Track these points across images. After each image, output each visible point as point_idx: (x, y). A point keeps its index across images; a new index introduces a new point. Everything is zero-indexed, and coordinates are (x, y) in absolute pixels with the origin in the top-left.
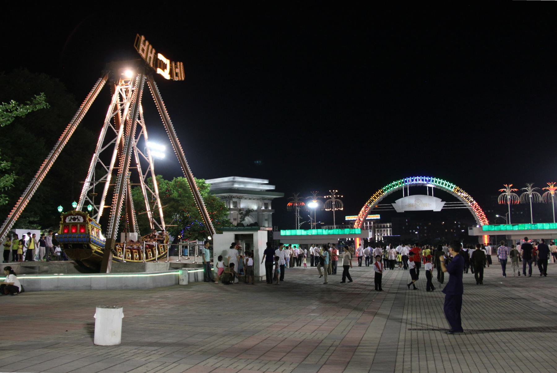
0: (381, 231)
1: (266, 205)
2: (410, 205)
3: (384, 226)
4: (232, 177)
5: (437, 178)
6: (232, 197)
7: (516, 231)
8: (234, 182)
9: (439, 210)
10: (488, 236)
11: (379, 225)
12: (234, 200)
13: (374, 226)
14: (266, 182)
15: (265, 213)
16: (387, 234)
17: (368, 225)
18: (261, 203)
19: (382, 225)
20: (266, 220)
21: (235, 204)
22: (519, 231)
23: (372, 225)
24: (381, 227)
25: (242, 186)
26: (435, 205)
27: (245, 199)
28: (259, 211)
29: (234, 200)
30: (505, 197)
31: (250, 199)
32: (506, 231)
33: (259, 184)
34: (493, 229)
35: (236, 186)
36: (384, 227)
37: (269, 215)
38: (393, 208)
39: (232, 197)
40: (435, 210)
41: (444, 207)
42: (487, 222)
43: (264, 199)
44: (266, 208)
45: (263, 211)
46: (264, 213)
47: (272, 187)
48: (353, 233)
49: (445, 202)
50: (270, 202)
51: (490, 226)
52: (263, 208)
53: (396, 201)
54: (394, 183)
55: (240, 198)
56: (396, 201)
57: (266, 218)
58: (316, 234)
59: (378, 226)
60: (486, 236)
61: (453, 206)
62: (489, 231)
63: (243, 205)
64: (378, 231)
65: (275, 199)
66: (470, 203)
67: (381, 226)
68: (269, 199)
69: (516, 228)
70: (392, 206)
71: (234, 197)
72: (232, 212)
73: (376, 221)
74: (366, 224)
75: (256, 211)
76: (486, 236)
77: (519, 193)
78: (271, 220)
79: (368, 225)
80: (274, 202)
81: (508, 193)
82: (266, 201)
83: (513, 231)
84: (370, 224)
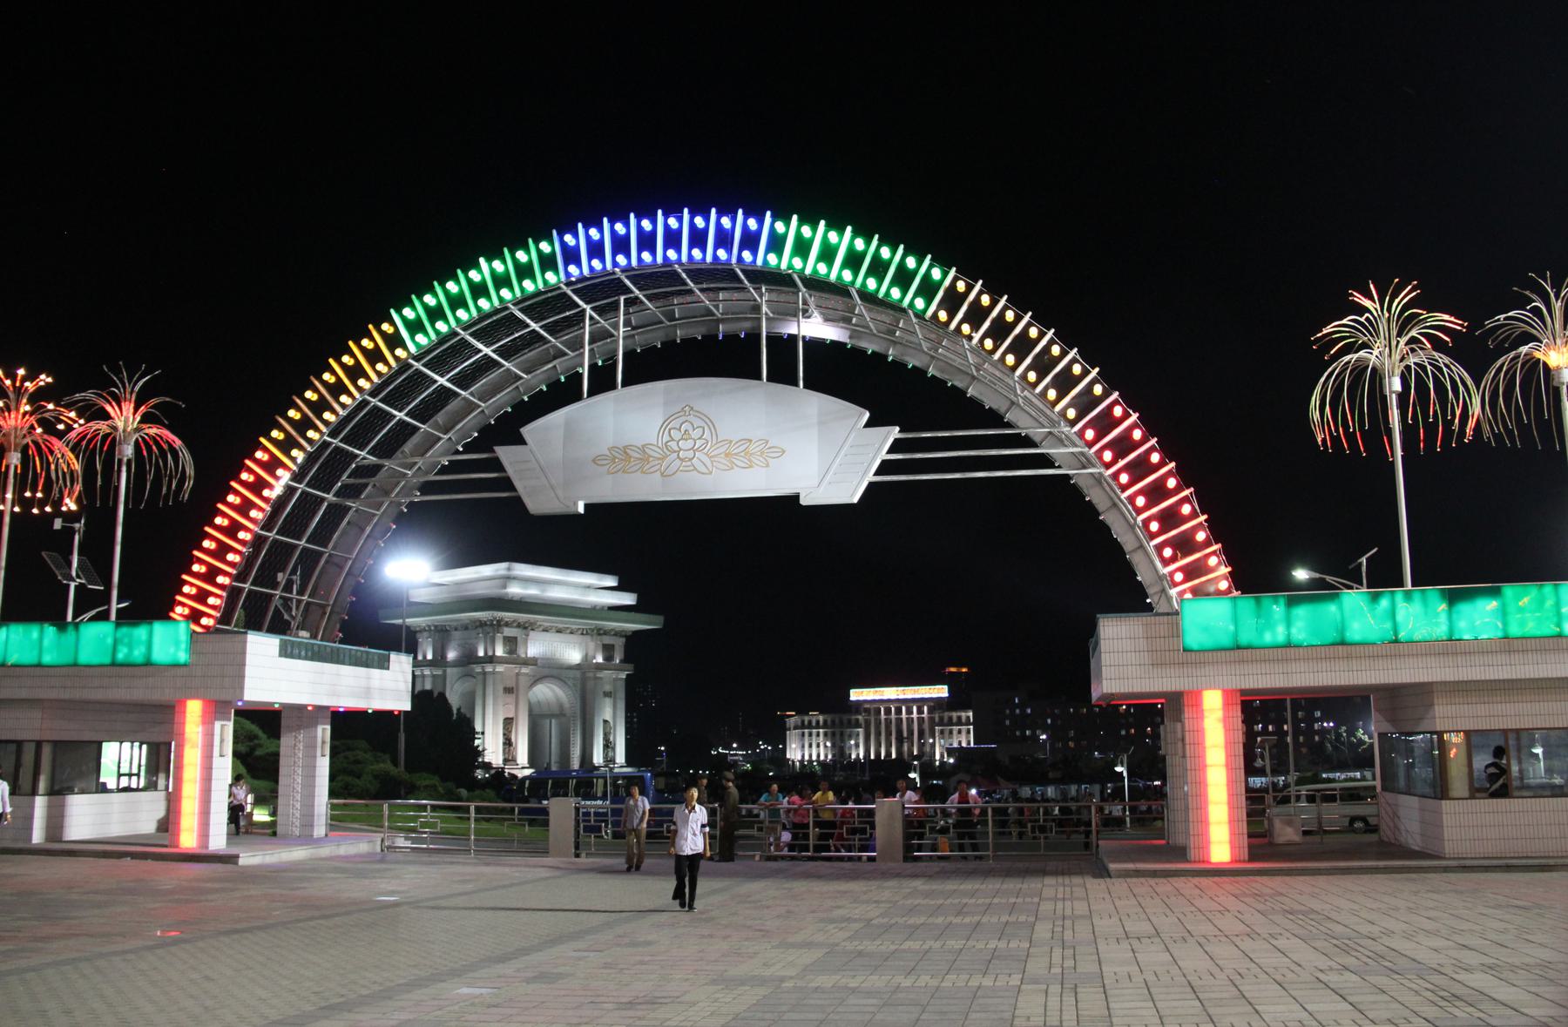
0: (951, 732)
1: (608, 650)
2: (625, 457)
3: (959, 718)
4: (504, 565)
5: (810, 219)
6: (499, 625)
7: (1477, 649)
8: (508, 579)
9: (850, 491)
10: (1227, 694)
11: (946, 714)
12: (508, 632)
13: (931, 719)
14: (611, 581)
15: (605, 674)
16: (888, 754)
17: (915, 715)
18: (592, 645)
19: (955, 715)
20: (607, 694)
21: (511, 642)
22: (1508, 645)
23: (925, 715)
24: (950, 723)
25: (532, 592)
26: (819, 455)
27: (545, 630)
28: (584, 668)
29: (508, 632)
30: (1367, 381)
31: (559, 631)
32: (1395, 646)
33: (589, 587)
34: (1278, 635)
35: (515, 590)
36: (959, 722)
37: (616, 680)
38: (507, 484)
39: (499, 625)
40: (813, 495)
41: (885, 468)
42: (1220, 572)
43: (601, 632)
44: (609, 658)
45: (599, 667)
46: (599, 675)
47: (628, 599)
48: (138, 655)
49: (894, 433)
50: (619, 643)
51: (1247, 603)
52: (600, 659)
53: (526, 431)
54: (484, 270)
55: (526, 627)
56: (526, 431)
57: (608, 688)
58: (28, 657)
59: (941, 719)
60: (1213, 701)
61: (957, 464)
62: (1238, 651)
63: (535, 647)
64: (942, 732)
65: (636, 633)
66: (1063, 417)
67: (950, 718)
68: (617, 634)
69: (1480, 617)
70: (496, 465)
71: (507, 625)
72: (500, 668)
73: (936, 704)
74: (909, 712)
75: (578, 667)
76: (1213, 701)
77: (1473, 351)
78: (621, 695)
79: (915, 715)
80: (634, 643)
81: (1387, 342)
82: (608, 640)
83: (1451, 646)
84: (920, 711)
